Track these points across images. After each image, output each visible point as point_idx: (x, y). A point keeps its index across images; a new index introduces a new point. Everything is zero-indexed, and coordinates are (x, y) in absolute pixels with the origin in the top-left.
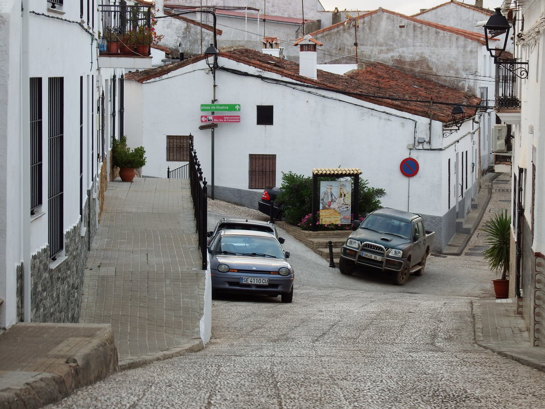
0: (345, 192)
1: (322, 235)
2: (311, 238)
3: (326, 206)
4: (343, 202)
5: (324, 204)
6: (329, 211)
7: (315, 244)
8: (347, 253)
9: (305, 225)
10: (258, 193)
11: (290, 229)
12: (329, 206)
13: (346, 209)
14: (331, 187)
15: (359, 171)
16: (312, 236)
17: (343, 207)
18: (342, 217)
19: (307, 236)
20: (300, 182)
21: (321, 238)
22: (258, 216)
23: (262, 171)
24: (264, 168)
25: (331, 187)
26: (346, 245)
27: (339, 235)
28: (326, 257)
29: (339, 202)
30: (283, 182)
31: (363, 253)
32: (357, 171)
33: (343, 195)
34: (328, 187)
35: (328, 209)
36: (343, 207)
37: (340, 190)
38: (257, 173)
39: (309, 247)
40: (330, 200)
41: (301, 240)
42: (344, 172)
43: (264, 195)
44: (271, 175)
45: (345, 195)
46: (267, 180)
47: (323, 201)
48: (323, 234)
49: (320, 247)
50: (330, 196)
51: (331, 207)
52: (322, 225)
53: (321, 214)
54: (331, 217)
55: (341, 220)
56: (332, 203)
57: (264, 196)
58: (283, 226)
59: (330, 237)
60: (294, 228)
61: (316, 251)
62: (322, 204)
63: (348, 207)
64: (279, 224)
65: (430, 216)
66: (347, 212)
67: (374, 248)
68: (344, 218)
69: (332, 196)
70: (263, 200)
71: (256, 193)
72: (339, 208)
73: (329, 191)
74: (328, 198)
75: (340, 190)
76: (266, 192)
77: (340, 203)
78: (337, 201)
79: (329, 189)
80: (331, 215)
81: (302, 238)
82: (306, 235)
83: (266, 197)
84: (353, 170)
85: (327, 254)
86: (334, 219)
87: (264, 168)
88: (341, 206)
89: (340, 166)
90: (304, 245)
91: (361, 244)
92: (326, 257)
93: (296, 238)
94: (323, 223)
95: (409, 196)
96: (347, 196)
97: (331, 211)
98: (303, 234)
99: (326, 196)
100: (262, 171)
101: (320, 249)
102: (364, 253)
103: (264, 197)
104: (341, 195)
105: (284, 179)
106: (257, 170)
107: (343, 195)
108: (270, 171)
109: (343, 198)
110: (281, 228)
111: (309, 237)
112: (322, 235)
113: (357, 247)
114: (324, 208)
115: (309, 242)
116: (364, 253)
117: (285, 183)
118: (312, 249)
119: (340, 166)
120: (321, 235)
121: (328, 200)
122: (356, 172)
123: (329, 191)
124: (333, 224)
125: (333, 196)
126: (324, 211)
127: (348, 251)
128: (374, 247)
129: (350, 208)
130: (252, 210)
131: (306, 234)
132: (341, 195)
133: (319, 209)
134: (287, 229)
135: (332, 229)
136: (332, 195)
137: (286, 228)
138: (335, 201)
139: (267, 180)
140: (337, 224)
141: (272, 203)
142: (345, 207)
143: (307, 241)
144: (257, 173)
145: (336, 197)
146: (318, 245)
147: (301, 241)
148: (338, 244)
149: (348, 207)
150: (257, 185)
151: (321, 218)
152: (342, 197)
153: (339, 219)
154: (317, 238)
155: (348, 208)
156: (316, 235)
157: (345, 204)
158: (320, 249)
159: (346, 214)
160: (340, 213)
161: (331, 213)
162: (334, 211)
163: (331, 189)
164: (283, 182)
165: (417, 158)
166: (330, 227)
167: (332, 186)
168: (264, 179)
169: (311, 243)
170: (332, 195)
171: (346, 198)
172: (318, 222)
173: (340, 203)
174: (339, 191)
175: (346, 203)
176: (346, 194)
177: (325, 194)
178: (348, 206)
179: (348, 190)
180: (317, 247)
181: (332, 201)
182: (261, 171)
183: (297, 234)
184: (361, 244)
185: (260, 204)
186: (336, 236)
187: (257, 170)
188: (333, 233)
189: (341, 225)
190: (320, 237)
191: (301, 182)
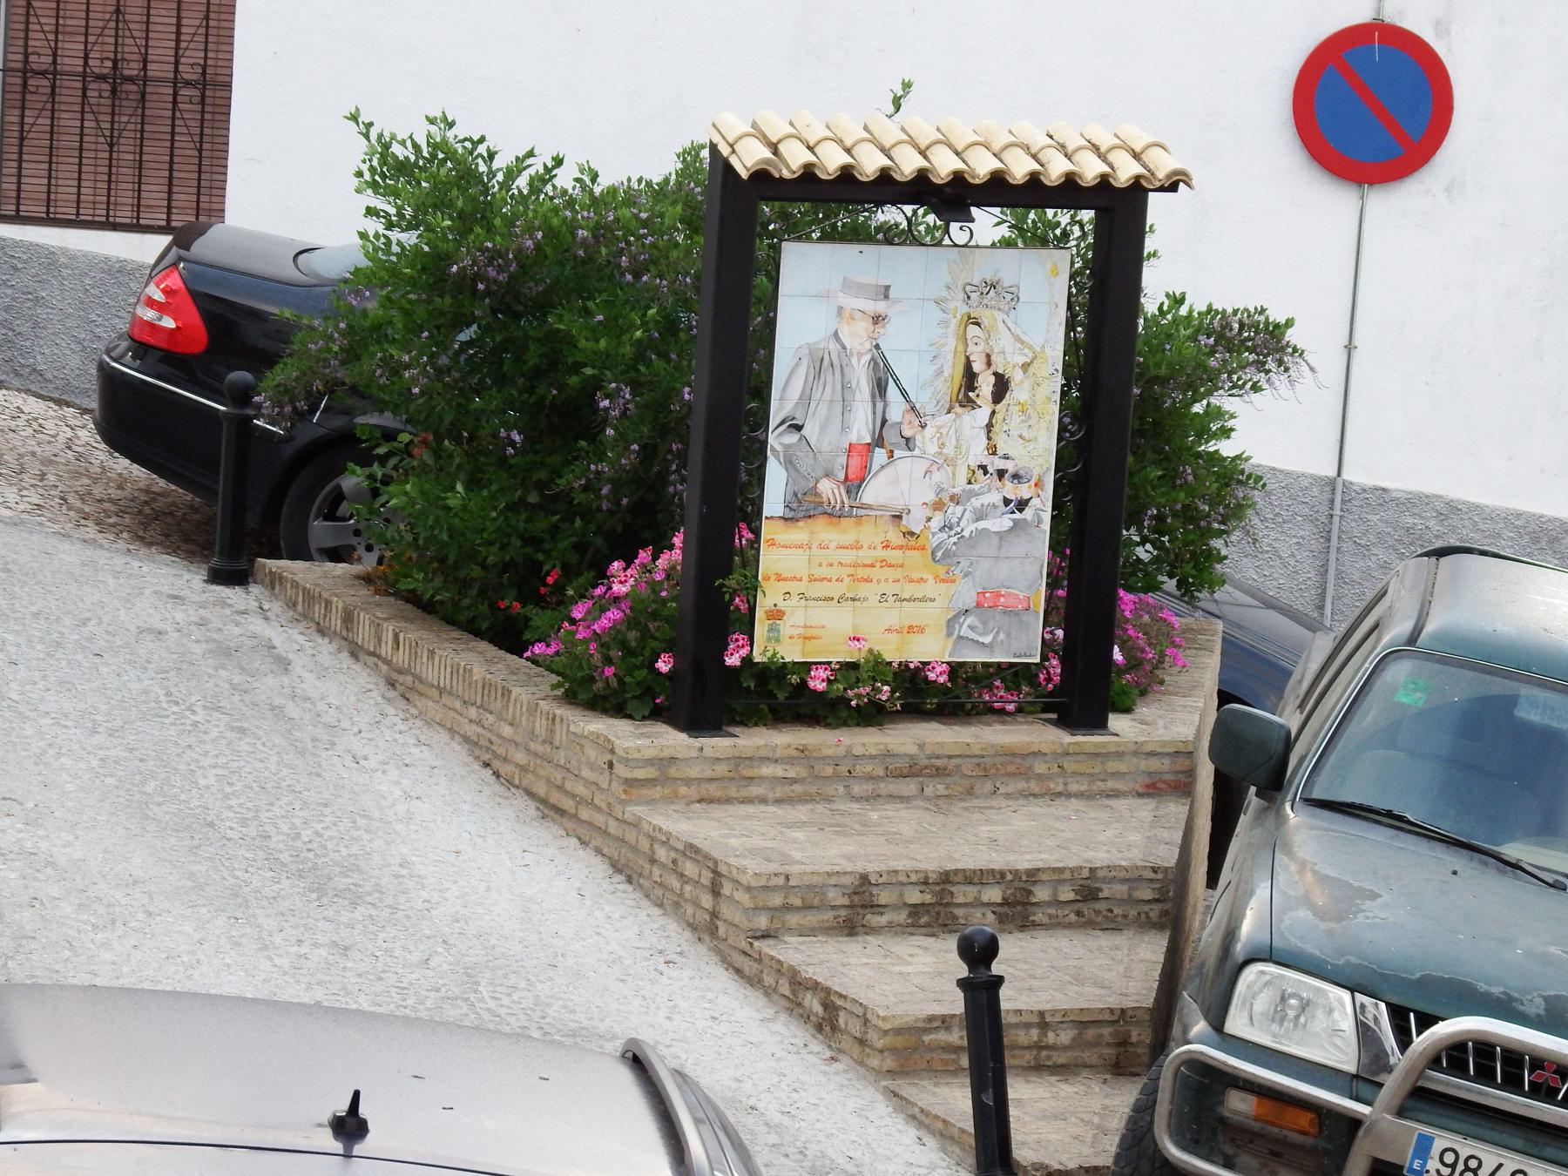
0: (1009, 360)
1: (778, 771)
2: (673, 798)
3: (827, 488)
4: (977, 452)
5: (805, 462)
6: (849, 538)
7: (742, 896)
8: (1223, 1121)
9: (608, 661)
10: (73, 257)
11: (431, 674)
12: (854, 484)
13: (1005, 523)
14: (880, 307)
15: (1163, 165)
16: (688, 782)
17: (976, 502)
18: (966, 594)
19: (630, 783)
20: (551, 233)
21: (763, 800)
22: (76, 475)
23: (115, 80)
24: (130, 50)
25: (880, 307)
26: (1218, 1024)
27: (939, 772)
28: (889, 1063)
29: (949, 450)
30: (370, 212)
31: (1424, 1147)
32: (1136, 156)
33: (986, 384)
34: (851, 302)
35: (834, 515)
36: (976, 502)
37: (964, 339)
38: (70, 91)
39: (669, 903)
40: (861, 431)
41: (568, 804)
42: (1056, 170)
43: (151, 303)
44: (190, 111)
45: (1001, 387)
46: (156, 153)
47: (792, 438)
48: (790, 761)
49: (793, 919)
50: (864, 388)
51: (870, 495)
52: (773, 674)
53: (770, 560)
54: (863, 590)
55: (950, 623)
56: (880, 455)
57: (149, 315)
58: (348, 618)
59: (857, 789)
60: (478, 672)
61: (748, 966)
62: (789, 463)
63: (1022, 505)
64: (309, 597)
65: (1519, 515)
66: (1019, 546)
67: (1512, 1083)
68: (986, 604)
69: (880, 388)
70: (144, 345)
71: (50, 259)
72: (938, 506)
73: (857, 337)
74: (846, 408)
75: (964, 339)
76: (174, 281)
77: (950, 462)
78: (927, 441)
79: (864, 326)
80: (859, 574)
81: (580, 790)
82: (620, 769)
83: (169, 323)
84: (1096, 149)
85: (898, 1031)
86: (894, 616)
87: (130, 50)
88: (961, 484)
89: (907, 86)
90: (600, 867)
91: (1404, 1041)
92: (889, 1063)
93: (505, 769)
94: (791, 653)
95: (1350, 348)
96: (1019, 392)
97: (871, 534)
98: (591, 752)
99: (828, 391)
100: (115, 80)
101: (798, 952)
102: (1442, 1140)
103: (151, 326)
104: (970, 377)
105: (374, 185)
106: (71, 60)
107: (986, 384)
108: (176, 82)
109: (982, 414)
110: (321, 631)
111: (656, 792)
112: (778, 771)
113: (1345, 1058)
114: (804, 508)
115: (662, 854)
116: (1438, 1146)
117: (390, 226)
118: (707, 929)
119: (907, 86)
120: (767, 770)
121: (844, 428)
122: (1125, 171)
123: (857, 337)
124: (878, 667)
125: (892, 390)
126: (799, 533)
127: (1239, 1104)
128: (1546, 1076)
129: (1042, 507)
130: (18, 399)
131: (626, 762)
132: (970, 377)
133: (752, 516)
134: (401, 658)
135: (873, 715)
136: (881, 383)
137: (386, 650)
138: (908, 442)
139: (156, 153)
140: (915, 657)
141: (242, 396)
142: (995, 498)
143: (631, 836)
144: (70, 91)
145: (921, 399)
146: (777, 900)
147: (562, 812)
148: (963, 894)
149: (1022, 505)
150: (66, 190)
151: (763, 604)
152: (968, 403)
153: (933, 614)
154: (728, 801)
155: (1028, 513)
156: (721, 770)
157: (1001, 474)
158: (798, 952)
159: (1003, 571)
160: (943, 558)
161: (866, 555)
162: (895, 537)
163: (877, 319)
164: (370, 212)
165: (1441, 26)
166: (858, 695)
167: (885, 292)
168: (127, 146)
169: (690, 869)
170: (881, 383)
171: (1016, 418)
172: (742, 639)
173: (950, 462)
174: (952, 343)
175: (1009, 466)
176: (1016, 377)
177: (819, 365)
178: (1024, 491)
179: (1036, 340)
180: (763, 922)
181: (879, 441)
182: (101, 78)
183: (507, 731)
184: (1404, 1041)
185: (112, 384)
186: (909, 787)
187: (71, 60)
188: (888, 754)
189: (955, 669)
190: (756, 790)
191: (557, 236)
